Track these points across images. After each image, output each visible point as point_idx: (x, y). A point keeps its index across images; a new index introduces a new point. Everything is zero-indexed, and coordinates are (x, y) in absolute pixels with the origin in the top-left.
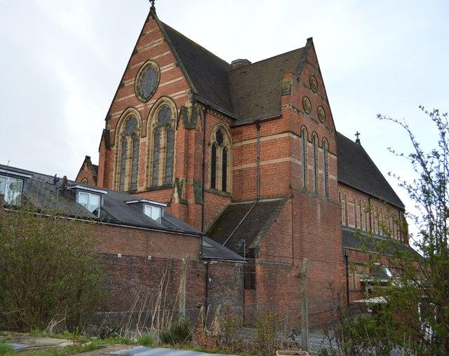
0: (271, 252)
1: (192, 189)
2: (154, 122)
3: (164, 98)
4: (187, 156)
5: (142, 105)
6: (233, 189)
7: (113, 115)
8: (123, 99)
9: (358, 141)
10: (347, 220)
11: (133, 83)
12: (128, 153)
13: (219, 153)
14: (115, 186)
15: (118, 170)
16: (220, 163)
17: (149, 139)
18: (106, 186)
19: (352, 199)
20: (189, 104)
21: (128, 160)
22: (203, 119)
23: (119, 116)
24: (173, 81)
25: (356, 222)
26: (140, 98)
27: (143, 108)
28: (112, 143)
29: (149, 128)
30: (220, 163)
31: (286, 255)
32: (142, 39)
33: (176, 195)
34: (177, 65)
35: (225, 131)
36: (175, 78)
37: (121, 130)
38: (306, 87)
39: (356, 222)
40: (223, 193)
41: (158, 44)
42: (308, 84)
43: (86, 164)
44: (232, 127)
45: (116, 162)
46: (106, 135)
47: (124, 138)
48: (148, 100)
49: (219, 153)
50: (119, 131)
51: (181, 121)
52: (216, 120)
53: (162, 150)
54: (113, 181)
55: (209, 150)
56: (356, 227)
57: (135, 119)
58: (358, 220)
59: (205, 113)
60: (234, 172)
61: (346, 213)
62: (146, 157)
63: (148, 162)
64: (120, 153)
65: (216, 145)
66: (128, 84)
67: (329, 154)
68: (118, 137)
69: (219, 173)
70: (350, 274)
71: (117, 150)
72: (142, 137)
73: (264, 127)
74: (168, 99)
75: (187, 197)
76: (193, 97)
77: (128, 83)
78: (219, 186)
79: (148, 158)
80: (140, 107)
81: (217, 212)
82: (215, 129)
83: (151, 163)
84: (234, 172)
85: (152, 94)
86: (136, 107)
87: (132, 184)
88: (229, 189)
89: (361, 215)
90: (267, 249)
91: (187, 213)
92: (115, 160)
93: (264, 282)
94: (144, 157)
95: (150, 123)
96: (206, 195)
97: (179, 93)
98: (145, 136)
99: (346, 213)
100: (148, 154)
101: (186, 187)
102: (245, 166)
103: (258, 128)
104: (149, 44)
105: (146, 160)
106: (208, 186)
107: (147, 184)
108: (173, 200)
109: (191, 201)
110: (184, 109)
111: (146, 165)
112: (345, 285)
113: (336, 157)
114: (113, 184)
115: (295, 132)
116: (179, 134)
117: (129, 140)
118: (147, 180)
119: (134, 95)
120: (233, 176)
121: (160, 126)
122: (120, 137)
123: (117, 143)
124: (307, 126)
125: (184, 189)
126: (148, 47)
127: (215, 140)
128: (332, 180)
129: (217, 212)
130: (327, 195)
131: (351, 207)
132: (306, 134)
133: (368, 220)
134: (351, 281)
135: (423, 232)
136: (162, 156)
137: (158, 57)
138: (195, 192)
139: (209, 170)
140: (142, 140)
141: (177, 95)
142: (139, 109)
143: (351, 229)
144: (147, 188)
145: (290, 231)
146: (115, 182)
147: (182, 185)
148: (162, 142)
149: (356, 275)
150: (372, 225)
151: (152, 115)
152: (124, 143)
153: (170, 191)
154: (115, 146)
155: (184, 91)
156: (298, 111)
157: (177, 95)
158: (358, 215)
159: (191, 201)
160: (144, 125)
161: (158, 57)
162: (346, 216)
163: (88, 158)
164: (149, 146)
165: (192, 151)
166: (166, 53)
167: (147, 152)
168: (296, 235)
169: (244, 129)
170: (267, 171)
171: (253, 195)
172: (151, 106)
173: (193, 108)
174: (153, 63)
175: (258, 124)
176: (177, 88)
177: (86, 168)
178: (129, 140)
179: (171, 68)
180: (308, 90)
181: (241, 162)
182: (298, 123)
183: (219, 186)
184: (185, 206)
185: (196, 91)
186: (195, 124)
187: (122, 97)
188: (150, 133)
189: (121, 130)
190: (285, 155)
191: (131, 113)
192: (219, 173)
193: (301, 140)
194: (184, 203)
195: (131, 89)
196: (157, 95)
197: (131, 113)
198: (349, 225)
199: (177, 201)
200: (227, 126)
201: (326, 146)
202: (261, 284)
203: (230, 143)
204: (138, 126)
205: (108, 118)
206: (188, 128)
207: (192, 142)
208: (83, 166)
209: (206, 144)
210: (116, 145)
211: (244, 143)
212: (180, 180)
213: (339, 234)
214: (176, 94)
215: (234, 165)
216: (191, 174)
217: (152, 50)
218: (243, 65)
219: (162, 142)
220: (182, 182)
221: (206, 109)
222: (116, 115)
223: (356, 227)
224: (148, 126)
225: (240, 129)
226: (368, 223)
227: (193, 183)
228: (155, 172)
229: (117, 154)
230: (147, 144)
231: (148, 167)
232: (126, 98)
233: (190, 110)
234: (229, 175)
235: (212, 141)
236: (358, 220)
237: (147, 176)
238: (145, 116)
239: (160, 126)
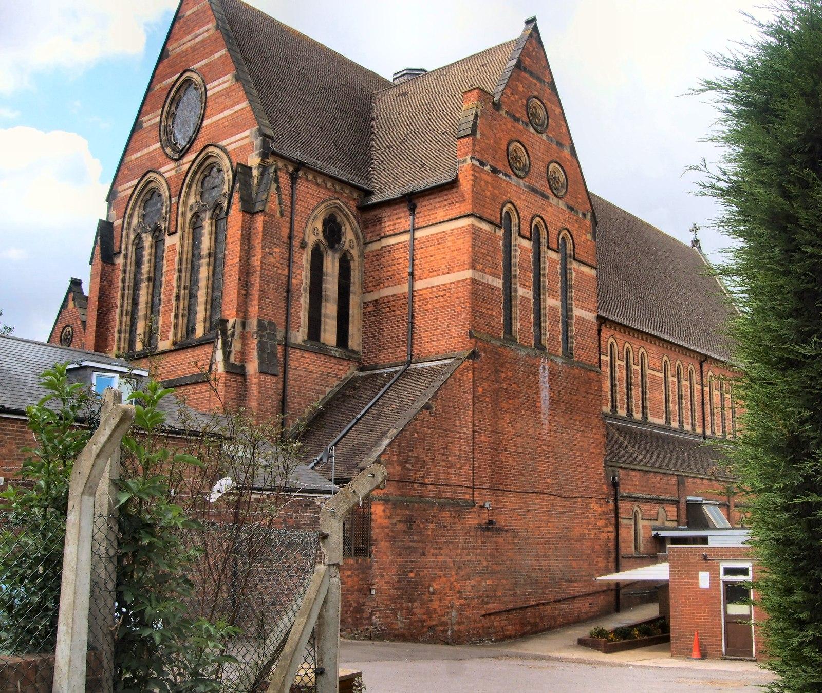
0: (414, 476)
1: (253, 343)
2: (192, 201)
3: (211, 149)
4: (246, 271)
5: (172, 165)
6: (364, 342)
7: (120, 189)
8: (139, 154)
9: (696, 242)
10: (644, 408)
11: (158, 119)
12: (145, 268)
13: (331, 266)
14: (119, 339)
15: (128, 307)
16: (331, 286)
17: (182, 238)
18: (213, 338)
19: (657, 364)
20: (254, 160)
21: (204, 261)
22: (287, 199)
23: (130, 191)
24: (227, 113)
25: (667, 412)
26: (168, 150)
27: (173, 172)
28: (116, 249)
29: (184, 214)
30: (331, 286)
31: (457, 480)
32: (177, 25)
33: (219, 355)
34: (237, 78)
35: (348, 220)
36: (233, 106)
37: (135, 221)
38: (517, 120)
39: (667, 412)
40: (337, 352)
41: (206, 35)
42: (522, 114)
43: (71, 296)
44: (364, 209)
45: (123, 289)
46: (105, 231)
47: (138, 237)
48: (183, 154)
49: (331, 266)
50: (129, 223)
51: (236, 196)
52: (323, 194)
53: (204, 261)
54: (116, 330)
55: (304, 259)
56: (668, 420)
57: (160, 195)
58: (674, 408)
59: (294, 178)
60: (366, 304)
61: (644, 393)
62: (175, 277)
63: (179, 287)
64: (131, 268)
65: (322, 248)
66: (149, 123)
67: (575, 265)
68: (128, 237)
69: (330, 309)
70: (623, 522)
71: (125, 265)
72: (170, 234)
73: (422, 207)
74: (217, 151)
75: (243, 361)
76: (264, 145)
77: (152, 120)
78: (329, 335)
79: (179, 279)
80: (169, 169)
81: (321, 392)
82: (321, 214)
83: (185, 288)
84: (366, 304)
85: (192, 142)
86: (162, 170)
87: (151, 335)
88: (354, 342)
89: (680, 397)
90: (404, 468)
91: (242, 395)
92: (120, 284)
93: (393, 540)
94: (170, 278)
95: (185, 202)
96: (295, 354)
97: (238, 137)
98: (176, 232)
99: (644, 393)
100: (180, 271)
101: (244, 338)
102: (386, 292)
103: (413, 210)
104: (189, 37)
105: (175, 283)
106: (300, 335)
107: (175, 335)
108: (214, 367)
109: (252, 367)
110: (241, 172)
111: (174, 294)
112: (612, 545)
113: (593, 272)
114: (116, 335)
115: (486, 216)
116: (236, 216)
117: (147, 240)
118: (176, 326)
119: (158, 145)
120: (365, 314)
121: (202, 209)
122: (132, 237)
123: (126, 248)
124: (518, 203)
125: (236, 346)
126: (186, 43)
127: (321, 237)
128: (581, 320)
129: (321, 392)
130: (568, 352)
131: (654, 379)
132: (515, 220)
133: (697, 407)
134: (626, 534)
135: (604, 435)
136: (204, 272)
137: (203, 63)
138: (261, 347)
139: (304, 300)
140: (169, 241)
141: (233, 142)
142: (167, 175)
143: (660, 427)
144: (175, 343)
145: (468, 430)
146: (120, 332)
147: (233, 335)
148: (206, 242)
149: (641, 523)
150: (708, 418)
151: (189, 186)
152: (139, 248)
153: (208, 349)
154: (122, 256)
155: (247, 133)
156: (495, 171)
157: (233, 142)
158: (674, 397)
159: (252, 367)
160: (174, 208)
161: (203, 63)
162: (644, 399)
163: (76, 284)
164: (181, 253)
165: (256, 260)
166: (218, 55)
167: (176, 267)
168: (483, 439)
169: (385, 213)
170: (427, 301)
171: (401, 354)
172: (187, 166)
173: (263, 167)
174: (195, 76)
175: (411, 201)
176: (235, 126)
177: (71, 305)
178: (147, 240)
179: (226, 85)
180: (520, 126)
181: (378, 284)
182: (494, 198)
183: (329, 335)
184: (239, 378)
185: (269, 132)
186: (265, 202)
187: (139, 150)
188: (184, 224)
189: (135, 221)
190: (462, 268)
191: (152, 185)
192: (330, 309)
193: (500, 233)
194: (237, 371)
195: (155, 133)
196: (199, 144)
197: (152, 185)
198: (651, 419)
199: (220, 368)
200: (348, 206)
201: (570, 246)
202: (384, 545)
203: (358, 244)
204: (164, 211)
205: (111, 197)
206: (249, 210)
207: (257, 242)
208: (66, 300)
209: (296, 243)
210: (123, 252)
211: (392, 241)
212: (229, 325)
213: (596, 435)
214: (233, 139)
215: (366, 290)
216: (254, 310)
217: (194, 49)
218: (415, 74)
219: (206, 242)
220: (234, 327)
221: (297, 170)
222: (126, 189)
223: (668, 420)
224: (181, 210)
225: (377, 212)
226: (698, 415)
227: (255, 329)
228: (191, 311)
229: (125, 272)
230: (177, 248)
231: (178, 298)
232: (145, 151)
233: (255, 172)
234: (354, 312)
235: (311, 240)
236: (674, 408)
237: (176, 317)
238: (180, 188)
239: (202, 209)
